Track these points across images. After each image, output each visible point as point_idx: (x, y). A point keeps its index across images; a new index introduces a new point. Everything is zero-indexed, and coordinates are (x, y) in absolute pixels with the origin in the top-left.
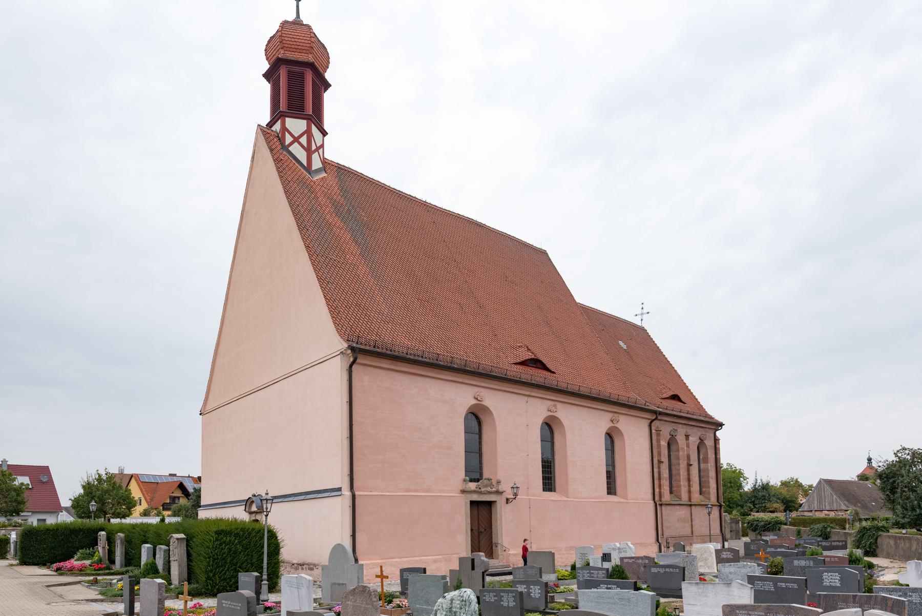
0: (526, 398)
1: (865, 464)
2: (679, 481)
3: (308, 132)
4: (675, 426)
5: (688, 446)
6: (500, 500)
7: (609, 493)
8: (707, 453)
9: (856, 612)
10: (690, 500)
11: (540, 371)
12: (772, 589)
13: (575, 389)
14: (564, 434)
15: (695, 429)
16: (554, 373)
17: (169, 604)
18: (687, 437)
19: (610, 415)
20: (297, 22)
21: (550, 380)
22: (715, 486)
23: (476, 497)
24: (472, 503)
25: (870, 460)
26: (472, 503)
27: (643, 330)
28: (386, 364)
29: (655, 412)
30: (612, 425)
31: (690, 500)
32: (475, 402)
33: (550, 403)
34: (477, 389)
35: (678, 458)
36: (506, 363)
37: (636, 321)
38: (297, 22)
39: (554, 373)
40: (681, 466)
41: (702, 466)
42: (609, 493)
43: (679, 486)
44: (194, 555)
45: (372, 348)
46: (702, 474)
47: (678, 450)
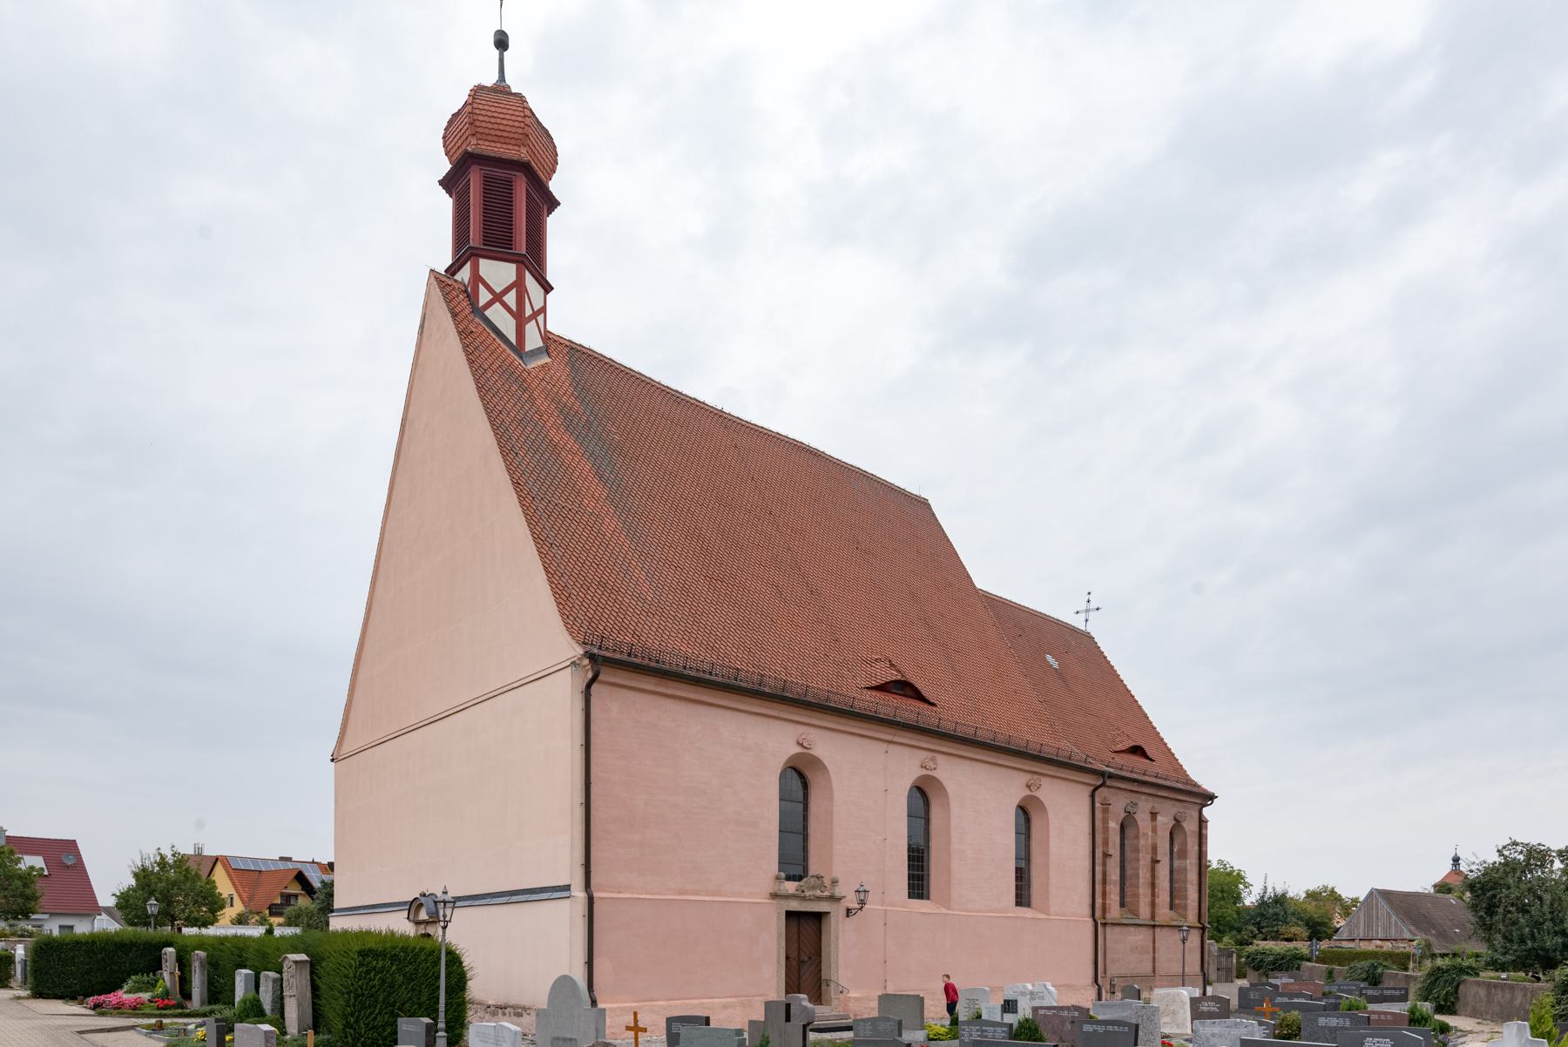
0: (885, 745)
3: (519, 285)
5: (1154, 830)
6: (836, 912)
7: (1018, 903)
10: (1153, 917)
14: (946, 806)
18: (1154, 815)
19: (1027, 777)
21: (926, 715)
23: (795, 906)
27: (1089, 638)
28: (648, 683)
31: (1153, 917)
33: (925, 754)
34: (801, 729)
36: (854, 687)
37: (1078, 622)
41: (1176, 863)
42: (1018, 903)
45: (625, 657)
47: (1137, 837)
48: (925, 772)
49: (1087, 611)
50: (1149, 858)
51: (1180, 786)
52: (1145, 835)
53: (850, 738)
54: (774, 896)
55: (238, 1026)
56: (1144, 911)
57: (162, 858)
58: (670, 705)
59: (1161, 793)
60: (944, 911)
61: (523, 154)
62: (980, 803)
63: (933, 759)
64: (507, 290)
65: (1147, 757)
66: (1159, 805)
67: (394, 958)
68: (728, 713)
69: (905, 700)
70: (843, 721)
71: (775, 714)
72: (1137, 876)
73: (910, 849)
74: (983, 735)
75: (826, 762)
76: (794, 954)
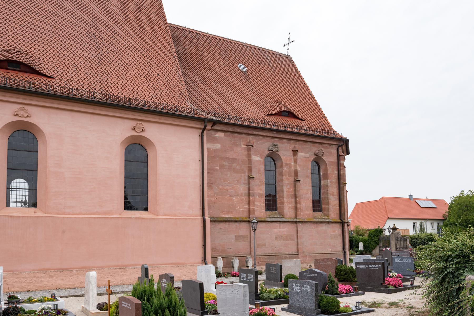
2: (283, 197)
4: (276, 141)
5: (295, 161)
7: (128, 206)
8: (326, 169)
9: (244, 287)
10: (296, 217)
11: (26, 75)
12: (299, 291)
14: (45, 142)
15: (308, 146)
16: (303, 120)
18: (295, 152)
21: (39, 83)
22: (337, 202)
27: (288, 58)
30: (134, 133)
31: (296, 217)
33: (17, 107)
35: (282, 174)
37: (283, 51)
39: (303, 120)
40: (286, 182)
41: (322, 182)
42: (128, 206)
46: (322, 191)
47: (281, 166)
50: (292, 179)
51: (326, 135)
52: (288, 165)
55: (297, 275)
56: (288, 212)
59: (314, 140)
62: (176, 154)
66: (298, 146)
69: (22, 74)
72: (282, 191)
73: (314, 201)
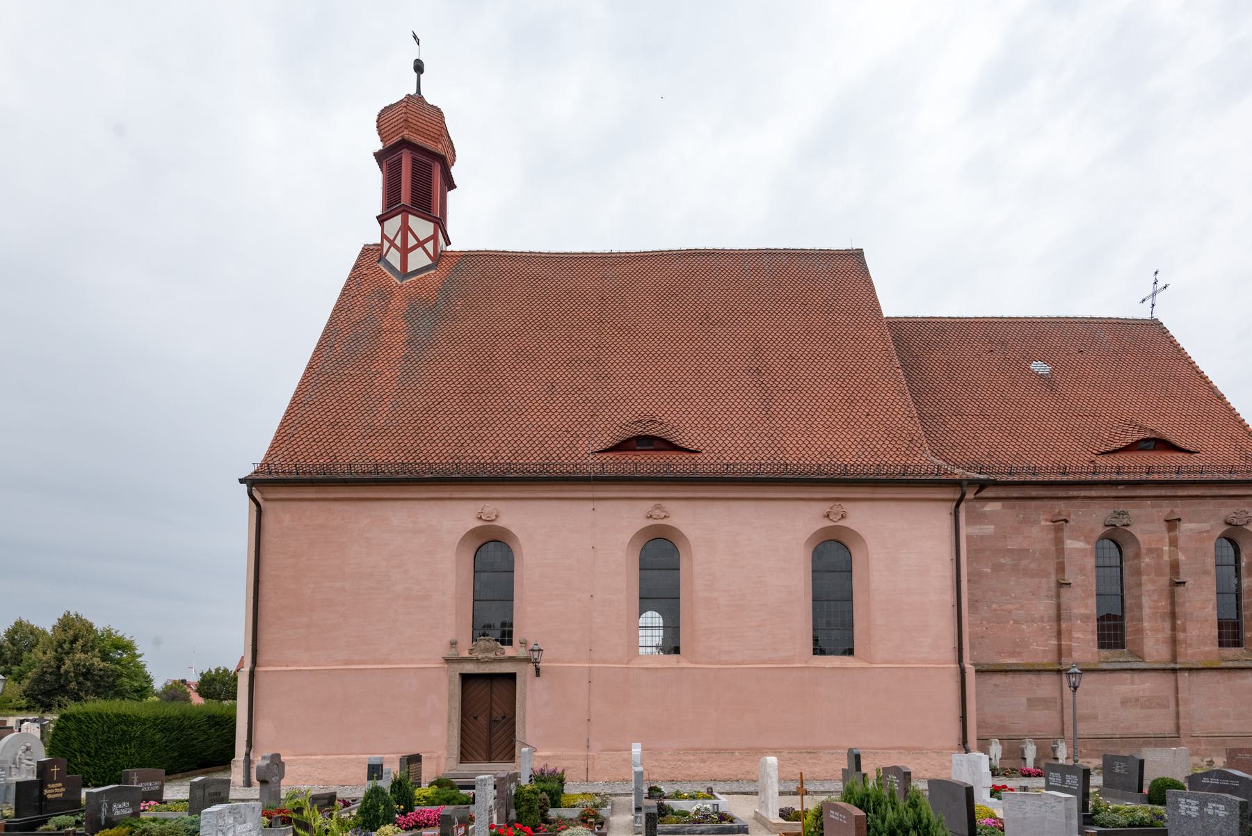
0: (591, 504)
1: (353, 207)
2: (1140, 620)
3: (434, 237)
6: (524, 674)
10: (1174, 659)
11: (662, 454)
13: (751, 471)
17: (1030, 764)
19: (825, 507)
20: (415, 101)
23: (470, 668)
24: (465, 678)
25: (416, 162)
26: (465, 678)
28: (310, 493)
29: (957, 484)
31: (1174, 659)
32: (479, 524)
33: (651, 504)
34: (481, 504)
36: (585, 453)
38: (415, 101)
43: (1140, 631)
44: (1182, 727)
45: (294, 476)
47: (1138, 555)
48: (652, 522)
49: (1154, 294)
53: (548, 503)
54: (447, 660)
56: (1154, 647)
57: (140, 656)
58: (338, 506)
60: (866, 665)
61: (439, 149)
63: (657, 507)
64: (427, 240)
65: (599, 452)
67: (79, 721)
68: (399, 503)
70: (523, 488)
71: (447, 495)
74: (341, 471)
75: (513, 530)
76: (137, 730)
